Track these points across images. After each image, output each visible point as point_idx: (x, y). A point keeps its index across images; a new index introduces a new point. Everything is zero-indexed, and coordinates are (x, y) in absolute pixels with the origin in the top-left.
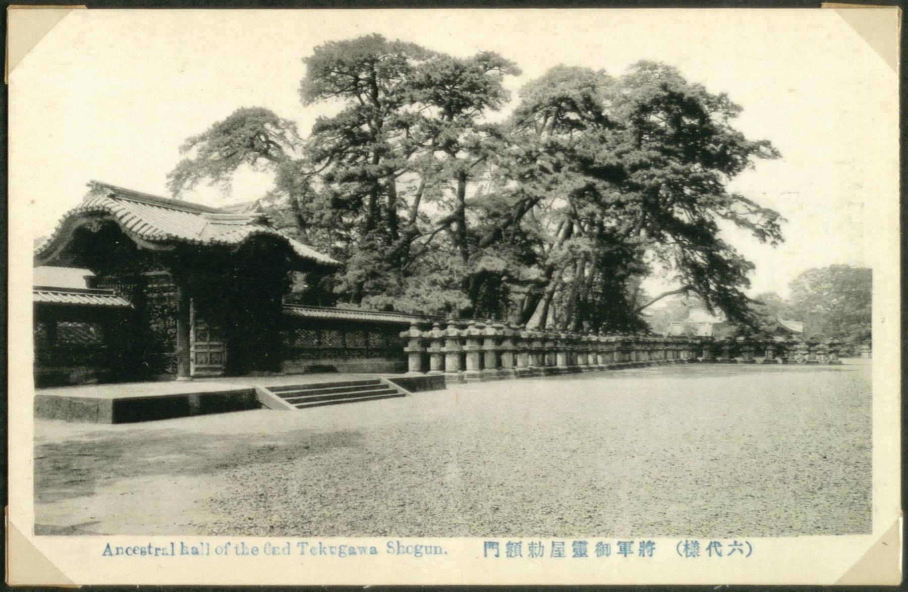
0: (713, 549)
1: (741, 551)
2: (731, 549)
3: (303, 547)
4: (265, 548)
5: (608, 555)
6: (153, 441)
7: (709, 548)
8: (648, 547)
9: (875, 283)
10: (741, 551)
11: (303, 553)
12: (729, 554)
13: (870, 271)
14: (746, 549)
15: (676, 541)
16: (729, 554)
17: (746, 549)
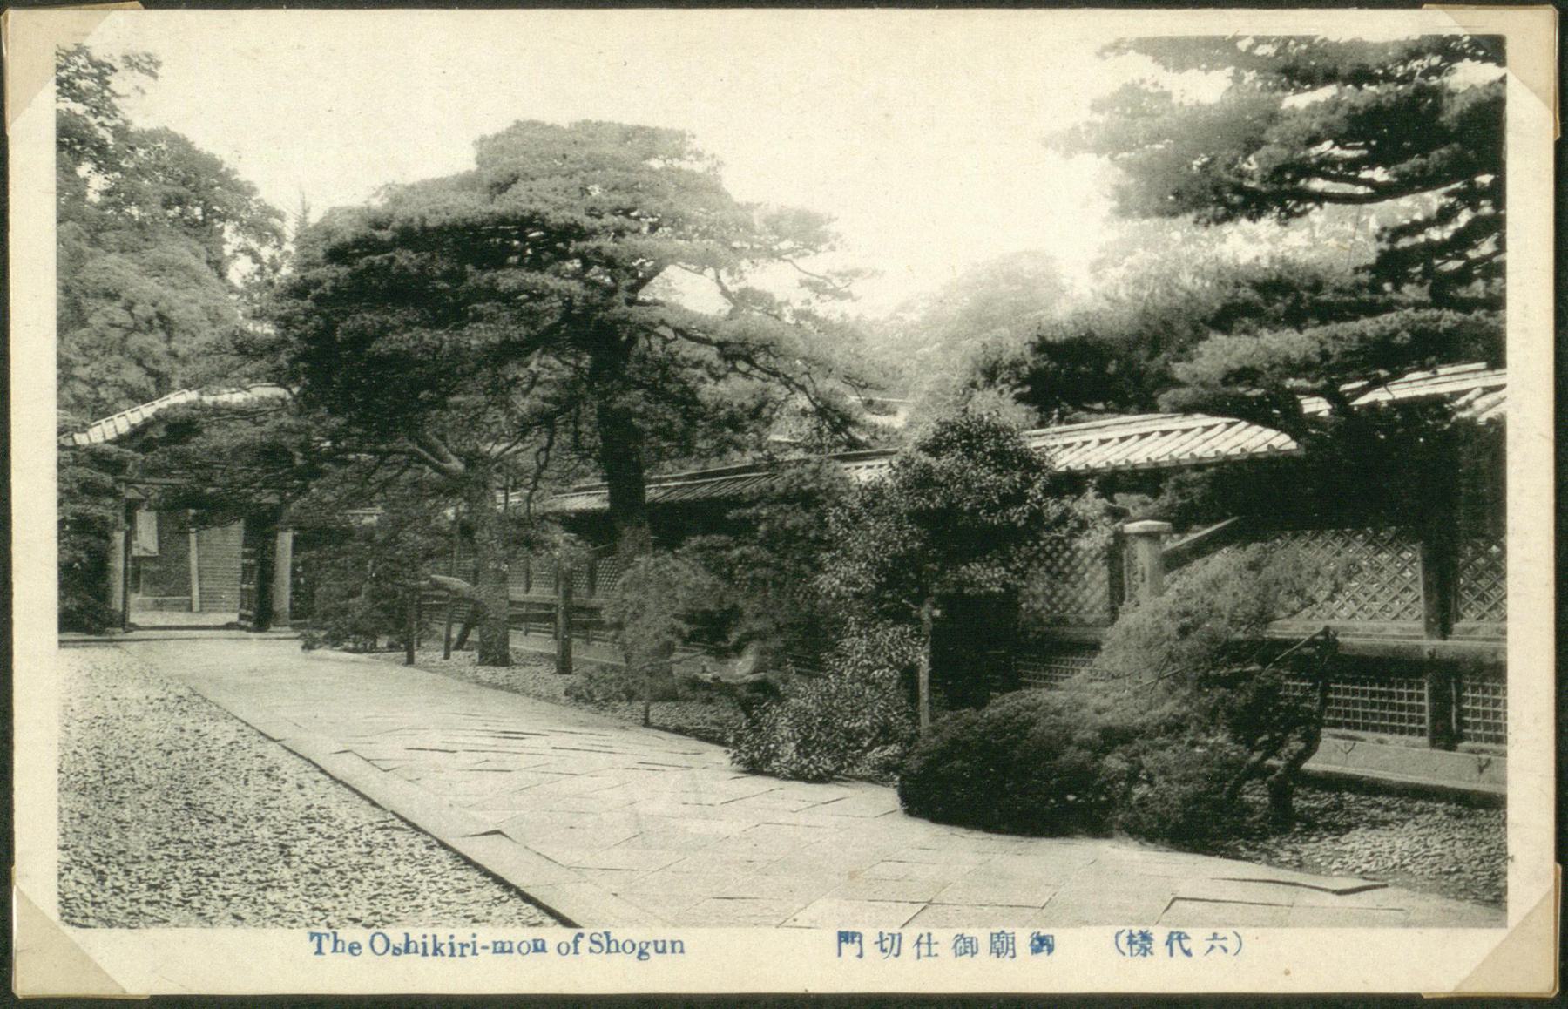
0: (1176, 944)
5: (973, 954)
6: (1450, 778)
11: (319, 952)
14: (1232, 944)
15: (1111, 931)
17: (1232, 944)
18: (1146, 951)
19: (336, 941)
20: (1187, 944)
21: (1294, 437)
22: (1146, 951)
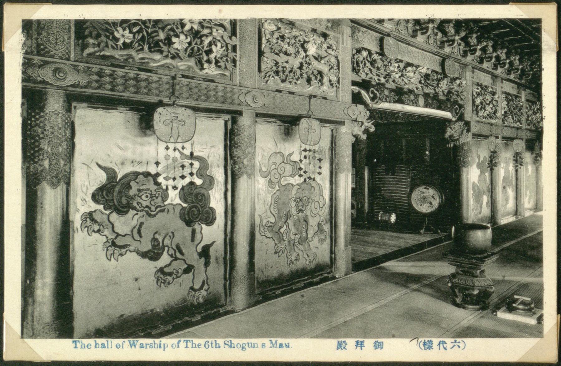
0: (441, 345)
1: (459, 347)
2: (453, 344)
3: (187, 343)
4: (205, 344)
5: (381, 348)
7: (439, 344)
8: (360, 345)
9: (544, 219)
10: (459, 347)
11: (187, 347)
12: (452, 348)
13: (23, 21)
16: (452, 348)
17: (462, 345)
18: (430, 347)
19: (192, 344)
20: (445, 345)
21: (368, 212)
22: (430, 347)
